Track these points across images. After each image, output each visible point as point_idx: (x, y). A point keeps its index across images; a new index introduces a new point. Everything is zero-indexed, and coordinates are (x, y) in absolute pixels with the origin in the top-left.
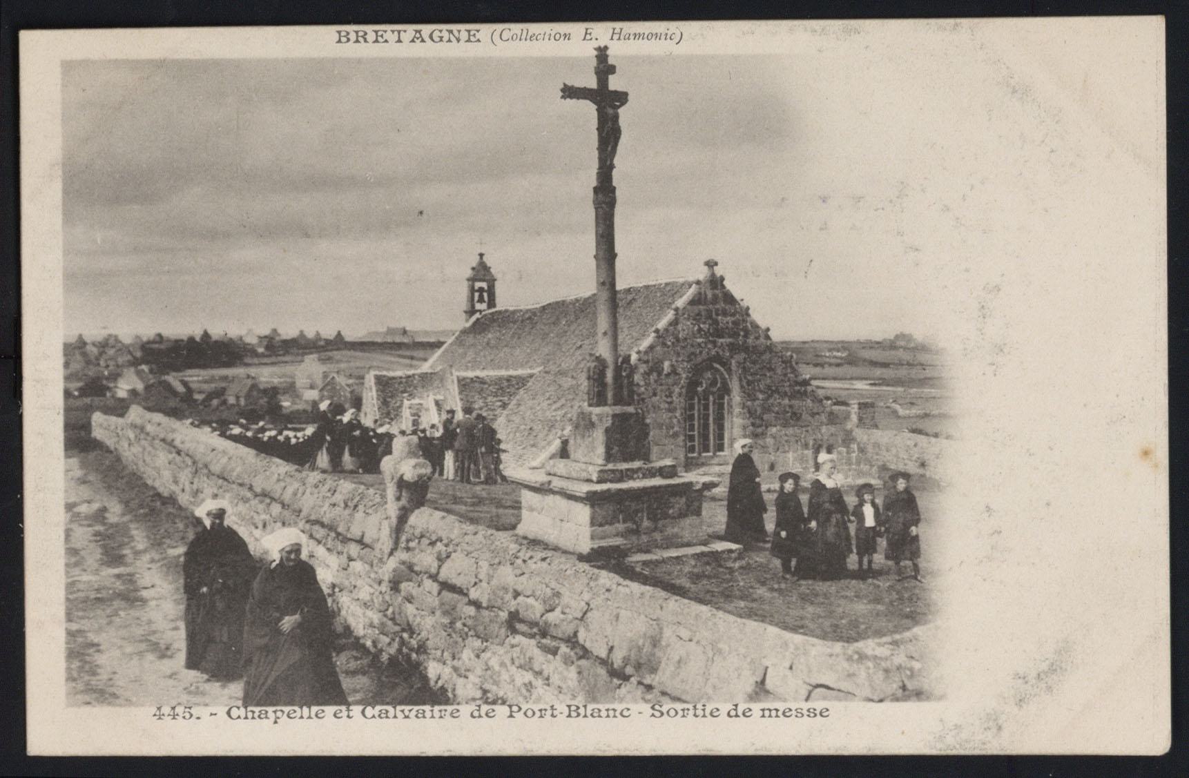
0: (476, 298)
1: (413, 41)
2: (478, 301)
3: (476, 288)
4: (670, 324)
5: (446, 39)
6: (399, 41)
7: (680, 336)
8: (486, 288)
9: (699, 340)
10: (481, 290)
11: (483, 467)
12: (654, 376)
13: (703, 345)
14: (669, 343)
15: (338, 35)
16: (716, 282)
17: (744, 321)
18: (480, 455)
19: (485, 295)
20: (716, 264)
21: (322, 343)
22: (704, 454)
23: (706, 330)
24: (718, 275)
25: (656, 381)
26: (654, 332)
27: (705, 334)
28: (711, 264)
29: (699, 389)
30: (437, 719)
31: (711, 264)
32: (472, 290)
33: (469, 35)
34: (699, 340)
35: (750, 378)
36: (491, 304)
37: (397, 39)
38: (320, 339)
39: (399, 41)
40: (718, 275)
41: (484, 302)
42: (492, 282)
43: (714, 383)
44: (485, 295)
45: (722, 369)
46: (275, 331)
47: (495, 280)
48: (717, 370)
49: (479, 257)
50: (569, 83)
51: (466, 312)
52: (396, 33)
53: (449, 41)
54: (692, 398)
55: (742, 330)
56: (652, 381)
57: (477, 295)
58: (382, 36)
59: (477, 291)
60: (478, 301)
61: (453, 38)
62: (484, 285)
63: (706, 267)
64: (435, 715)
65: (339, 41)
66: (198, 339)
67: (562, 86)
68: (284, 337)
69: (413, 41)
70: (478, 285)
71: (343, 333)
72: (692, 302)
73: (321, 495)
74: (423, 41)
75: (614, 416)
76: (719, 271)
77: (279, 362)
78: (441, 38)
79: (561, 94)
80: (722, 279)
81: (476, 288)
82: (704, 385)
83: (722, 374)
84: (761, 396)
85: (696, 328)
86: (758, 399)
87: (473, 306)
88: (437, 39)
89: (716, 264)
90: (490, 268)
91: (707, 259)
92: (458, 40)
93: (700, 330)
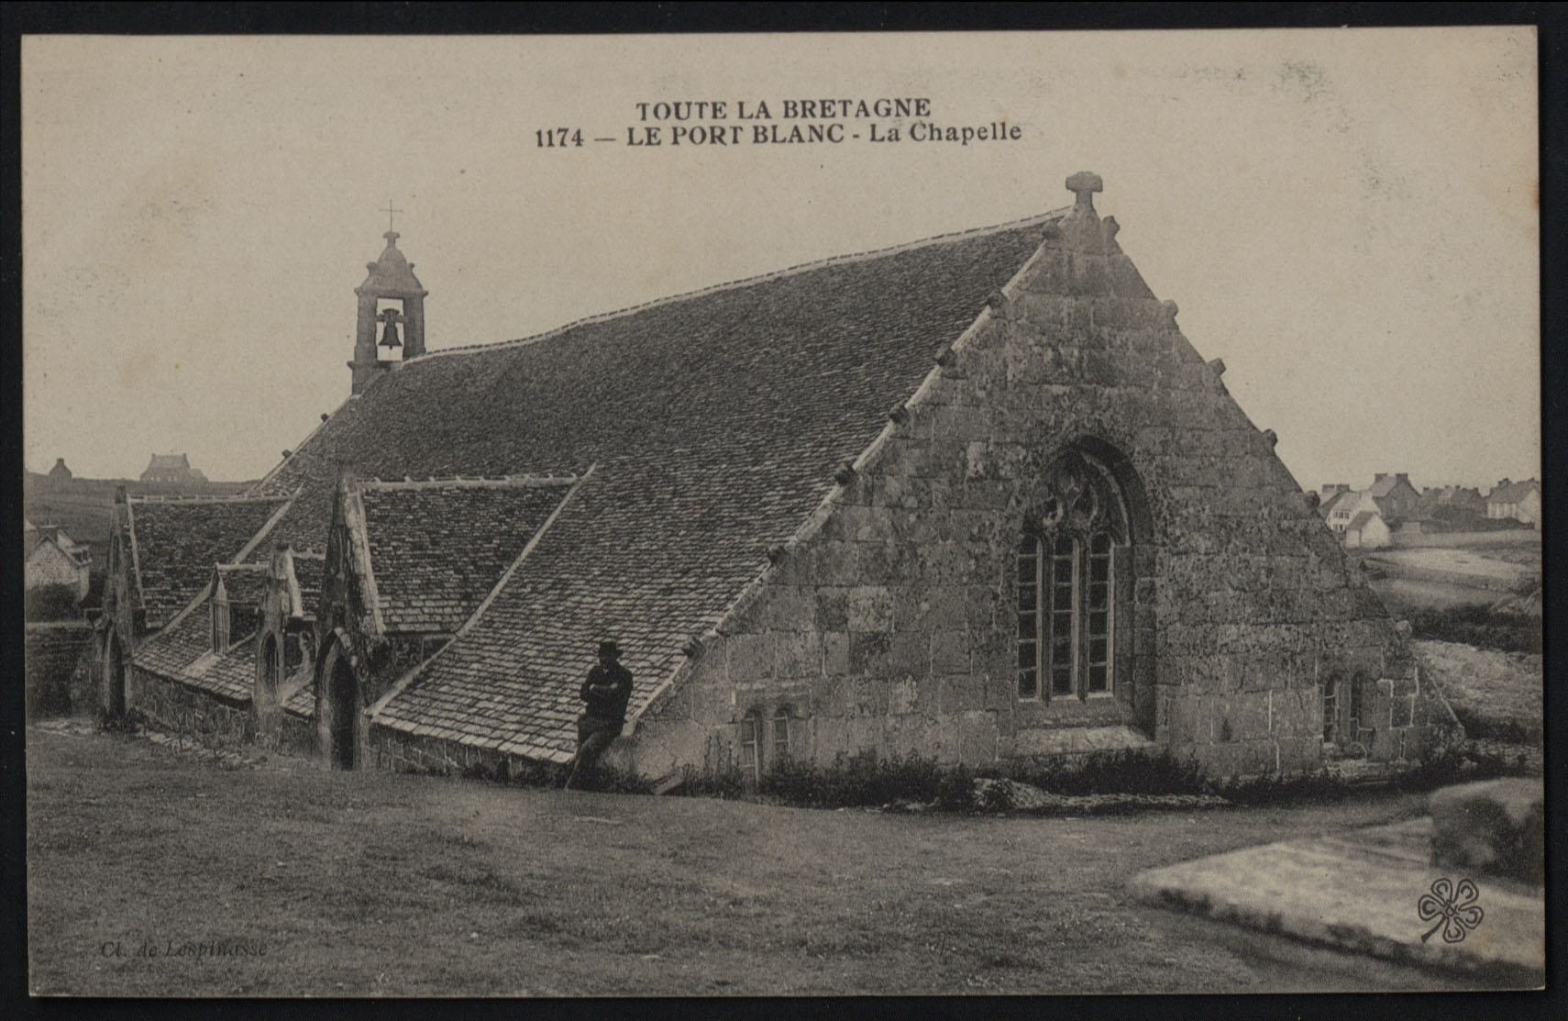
0: (380, 336)
3: (380, 312)
5: (893, 112)
9: (1057, 389)
12: (939, 487)
18: (365, 734)
22: (1091, 696)
25: (947, 499)
27: (1071, 372)
28: (1084, 187)
30: (683, 102)
34: (1057, 389)
45: (1104, 470)
48: (1094, 472)
49: (385, 243)
56: (937, 496)
57: (381, 327)
64: (686, 107)
70: (384, 305)
73: (1197, 462)
77: (1148, 807)
84: (1203, 543)
85: (1049, 354)
93: (1058, 362)
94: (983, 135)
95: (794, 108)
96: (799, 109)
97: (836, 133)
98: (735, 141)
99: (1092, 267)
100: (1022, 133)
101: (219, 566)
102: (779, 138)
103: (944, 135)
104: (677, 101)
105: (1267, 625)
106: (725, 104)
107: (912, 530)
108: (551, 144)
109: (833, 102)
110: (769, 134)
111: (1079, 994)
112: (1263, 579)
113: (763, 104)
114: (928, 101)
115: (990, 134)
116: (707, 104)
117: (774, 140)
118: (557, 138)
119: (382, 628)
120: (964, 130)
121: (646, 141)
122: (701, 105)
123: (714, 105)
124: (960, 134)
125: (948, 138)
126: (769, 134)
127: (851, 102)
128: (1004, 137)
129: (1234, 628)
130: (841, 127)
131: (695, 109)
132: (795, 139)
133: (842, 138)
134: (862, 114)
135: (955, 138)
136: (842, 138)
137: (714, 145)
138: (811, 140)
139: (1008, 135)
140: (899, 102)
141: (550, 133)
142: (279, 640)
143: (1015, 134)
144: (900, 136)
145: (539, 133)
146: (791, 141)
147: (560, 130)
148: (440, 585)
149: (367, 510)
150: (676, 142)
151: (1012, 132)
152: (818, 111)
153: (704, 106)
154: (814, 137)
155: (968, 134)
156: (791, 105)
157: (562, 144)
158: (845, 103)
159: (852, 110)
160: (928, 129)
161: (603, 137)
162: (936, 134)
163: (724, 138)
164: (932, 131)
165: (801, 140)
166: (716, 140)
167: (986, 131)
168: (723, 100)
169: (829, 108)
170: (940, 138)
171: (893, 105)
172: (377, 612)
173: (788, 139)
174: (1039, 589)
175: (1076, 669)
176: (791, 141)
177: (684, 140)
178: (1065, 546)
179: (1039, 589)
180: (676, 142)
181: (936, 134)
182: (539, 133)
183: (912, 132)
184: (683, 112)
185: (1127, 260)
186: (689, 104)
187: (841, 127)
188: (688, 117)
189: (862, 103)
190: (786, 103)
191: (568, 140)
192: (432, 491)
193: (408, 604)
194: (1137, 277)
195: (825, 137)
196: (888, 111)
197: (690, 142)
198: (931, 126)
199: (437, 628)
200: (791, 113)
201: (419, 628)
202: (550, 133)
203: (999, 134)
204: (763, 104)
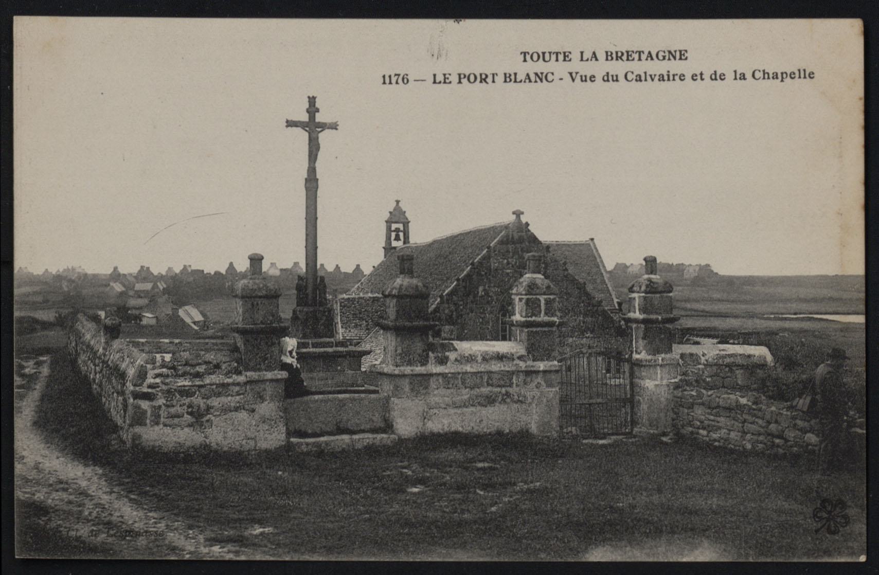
2: (395, 239)
3: (393, 228)
5: (667, 58)
8: (402, 229)
10: (397, 230)
11: (671, 313)
13: (511, 275)
14: (483, 273)
19: (401, 234)
20: (522, 213)
23: (513, 263)
24: (524, 222)
27: (513, 266)
28: (518, 214)
31: (518, 214)
32: (389, 230)
34: (509, 271)
36: (406, 240)
40: (524, 222)
41: (400, 240)
42: (406, 224)
44: (401, 234)
47: (409, 222)
49: (395, 203)
57: (393, 235)
59: (394, 231)
60: (395, 239)
62: (401, 226)
66: (223, 272)
68: (249, 266)
70: (394, 226)
71: (361, 267)
76: (524, 219)
80: (527, 224)
81: (393, 228)
85: (506, 261)
88: (661, 58)
89: (522, 213)
90: (405, 212)
93: (508, 263)
94: (793, 76)
95: (611, 55)
96: (614, 56)
97: (550, 77)
98: (493, 82)
100: (815, 75)
103: (771, 76)
104: (544, 51)
106: (686, 51)
107: (462, 310)
108: (390, 83)
109: (633, 52)
110: (513, 77)
112: (582, 324)
113: (594, 53)
114: (570, 53)
115: (797, 75)
116: (560, 53)
117: (515, 81)
118: (394, 80)
119: (341, 338)
120: (782, 73)
121: (443, 81)
122: (557, 54)
123: (565, 53)
124: (779, 76)
125: (773, 78)
126: (513, 77)
127: (643, 52)
128: (805, 77)
129: (571, 339)
130: (553, 74)
131: (554, 57)
132: (527, 81)
133: (553, 80)
134: (649, 59)
135: (777, 78)
136: (553, 80)
137: (481, 84)
138: (536, 82)
139: (718, 77)
140: (670, 52)
141: (390, 77)
143: (811, 76)
144: (746, 77)
145: (384, 77)
146: (525, 82)
147: (396, 75)
148: (360, 325)
150: (460, 82)
151: (720, 76)
152: (625, 57)
153: (559, 54)
154: (538, 80)
155: (784, 75)
156: (609, 54)
157: (397, 83)
158: (640, 52)
159: (644, 57)
160: (762, 73)
161: (419, 82)
163: (487, 80)
164: (764, 74)
165: (530, 81)
166: (483, 81)
167: (794, 74)
168: (569, 50)
169: (631, 56)
170: (769, 78)
171: (667, 54)
172: (341, 334)
173: (523, 80)
176: (525, 82)
177: (465, 81)
180: (460, 82)
182: (384, 77)
183: (753, 76)
184: (547, 58)
186: (550, 53)
187: (553, 74)
188: (550, 59)
189: (650, 53)
190: (607, 52)
191: (400, 81)
193: (350, 331)
196: (664, 58)
197: (467, 82)
198: (764, 71)
199: (358, 338)
200: (609, 58)
201: (352, 338)
202: (390, 77)
203: (802, 76)
204: (594, 53)
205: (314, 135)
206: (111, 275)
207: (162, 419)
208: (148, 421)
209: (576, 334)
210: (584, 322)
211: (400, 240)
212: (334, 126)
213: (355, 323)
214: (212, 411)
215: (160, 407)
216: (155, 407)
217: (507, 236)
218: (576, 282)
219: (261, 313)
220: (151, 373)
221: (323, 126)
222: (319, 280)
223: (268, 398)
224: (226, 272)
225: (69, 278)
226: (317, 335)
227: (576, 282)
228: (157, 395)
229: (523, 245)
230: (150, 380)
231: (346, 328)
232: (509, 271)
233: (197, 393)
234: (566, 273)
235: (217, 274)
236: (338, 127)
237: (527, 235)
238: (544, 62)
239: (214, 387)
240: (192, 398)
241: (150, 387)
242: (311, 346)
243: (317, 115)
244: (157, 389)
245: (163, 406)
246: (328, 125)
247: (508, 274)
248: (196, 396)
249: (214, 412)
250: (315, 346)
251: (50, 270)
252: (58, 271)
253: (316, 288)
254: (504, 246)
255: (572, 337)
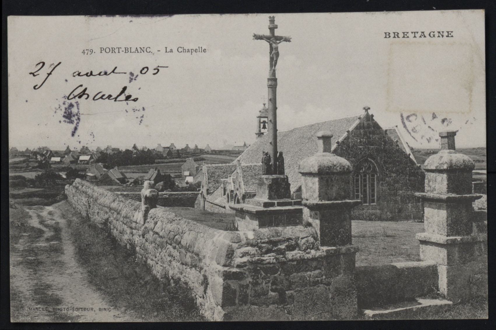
0: (262, 126)
1: (420, 37)
2: (263, 128)
3: (262, 121)
4: (345, 139)
6: (415, 37)
7: (350, 145)
13: (362, 149)
14: (344, 148)
15: (385, 34)
16: (369, 118)
17: (384, 137)
20: (369, 108)
21: (199, 151)
22: (372, 204)
26: (337, 143)
28: (367, 109)
29: (361, 171)
31: (367, 109)
32: (260, 122)
33: (448, 34)
34: (361, 147)
35: (387, 166)
37: (414, 36)
38: (198, 149)
39: (415, 37)
41: (266, 128)
43: (369, 168)
46: (172, 144)
48: (371, 162)
50: (256, 33)
51: (256, 134)
52: (414, 33)
53: (439, 36)
54: (357, 176)
55: (383, 141)
57: (262, 125)
58: (406, 35)
59: (262, 123)
60: (263, 128)
61: (440, 35)
63: (364, 110)
65: (386, 37)
67: (253, 35)
69: (420, 37)
70: (262, 120)
72: (357, 128)
74: (425, 37)
75: (273, 179)
76: (370, 112)
78: (434, 36)
79: (253, 38)
80: (372, 116)
82: (364, 169)
83: (374, 164)
85: (359, 140)
86: (392, 177)
87: (260, 131)
88: (432, 36)
91: (364, 107)
92: (443, 36)
93: (361, 142)
99: (368, 124)
101: (221, 179)
102: (132, 51)
105: (409, 191)
111: (173, 321)
112: (408, 182)
115: (198, 51)
117: (131, 52)
124: (190, 51)
139: (203, 51)
142: (229, 194)
149: (242, 169)
154: (142, 51)
155: (192, 51)
162: (184, 51)
174: (360, 184)
175: (368, 200)
178: (365, 176)
179: (360, 184)
181: (184, 51)
183: (430, 35)
185: (376, 122)
192: (256, 166)
194: (378, 125)
195: (145, 51)
203: (200, 51)
205: (274, 45)
206: (65, 151)
207: (250, 297)
208: (237, 301)
209: (404, 188)
210: (409, 180)
211: (266, 128)
212: (287, 40)
213: (252, 182)
214: (293, 286)
215: (247, 286)
216: (243, 285)
217: (360, 124)
218: (404, 154)
219: (335, 189)
220: (238, 252)
221: (280, 39)
222: (278, 154)
223: (342, 271)
224: (81, 150)
225: (41, 153)
226: (280, 197)
227: (404, 154)
228: (245, 274)
229: (370, 130)
230: (238, 260)
231: (247, 185)
232: (361, 147)
233: (280, 269)
234: (397, 147)
235: (127, 151)
236: (291, 40)
237: (373, 123)
238: (89, 95)
239: (295, 263)
240: (276, 275)
241: (238, 266)
242: (276, 204)
243: (276, 30)
244: (245, 268)
245: (250, 285)
246: (284, 38)
247: (360, 149)
248: (279, 273)
249: (296, 288)
250: (279, 204)
251: (29, 149)
252: (34, 149)
253: (276, 159)
254: (358, 130)
255: (402, 190)
